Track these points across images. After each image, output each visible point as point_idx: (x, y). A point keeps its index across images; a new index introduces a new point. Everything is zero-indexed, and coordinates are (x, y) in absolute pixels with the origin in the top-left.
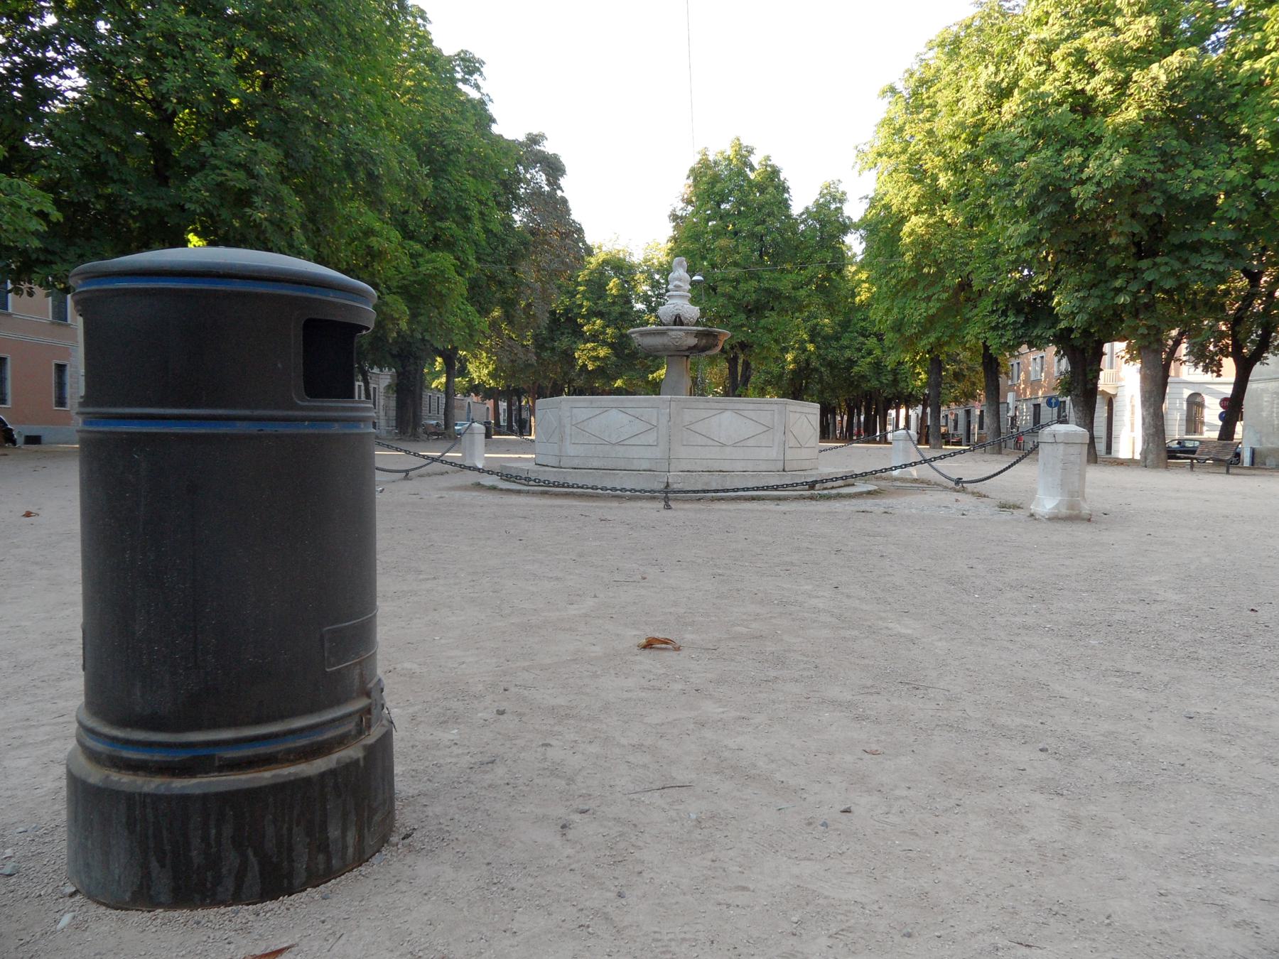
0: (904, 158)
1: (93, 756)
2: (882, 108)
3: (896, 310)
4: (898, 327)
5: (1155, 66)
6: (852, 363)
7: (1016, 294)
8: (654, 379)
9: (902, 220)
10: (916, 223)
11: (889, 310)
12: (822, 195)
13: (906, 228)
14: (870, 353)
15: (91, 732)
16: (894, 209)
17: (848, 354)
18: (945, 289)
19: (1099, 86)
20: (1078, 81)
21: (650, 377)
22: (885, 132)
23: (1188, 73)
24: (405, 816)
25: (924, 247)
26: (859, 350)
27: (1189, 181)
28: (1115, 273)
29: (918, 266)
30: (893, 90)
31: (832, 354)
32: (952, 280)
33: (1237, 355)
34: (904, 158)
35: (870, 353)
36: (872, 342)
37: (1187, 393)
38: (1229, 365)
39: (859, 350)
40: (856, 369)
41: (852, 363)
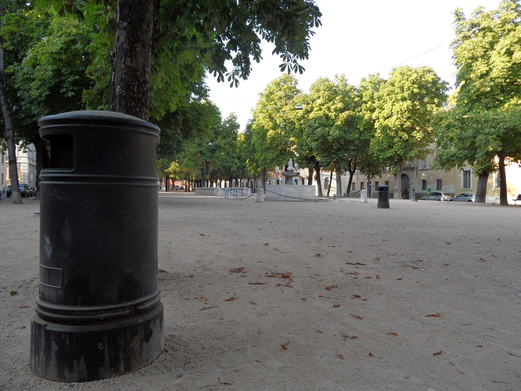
0: (267, 114)
1: (42, 317)
2: (257, 99)
3: (264, 155)
4: (265, 160)
5: (343, 113)
6: (231, 167)
7: (307, 156)
8: (167, 172)
9: (267, 131)
10: (271, 131)
11: (261, 156)
12: (230, 116)
13: (268, 134)
14: (236, 164)
15: (41, 307)
16: (265, 128)
17: (229, 164)
18: (278, 150)
19: (332, 115)
20: (327, 112)
21: (166, 171)
22: (261, 105)
23: (349, 116)
24: (175, 313)
25: (273, 139)
26: (233, 163)
27: (350, 137)
28: (333, 154)
29: (271, 144)
30: (262, 94)
31: (225, 164)
32: (280, 148)
33: (350, 171)
34: (267, 114)
35: (236, 164)
36: (236, 160)
37: (325, 177)
38: (348, 173)
39: (233, 163)
40: (232, 169)
41: (231, 167)
